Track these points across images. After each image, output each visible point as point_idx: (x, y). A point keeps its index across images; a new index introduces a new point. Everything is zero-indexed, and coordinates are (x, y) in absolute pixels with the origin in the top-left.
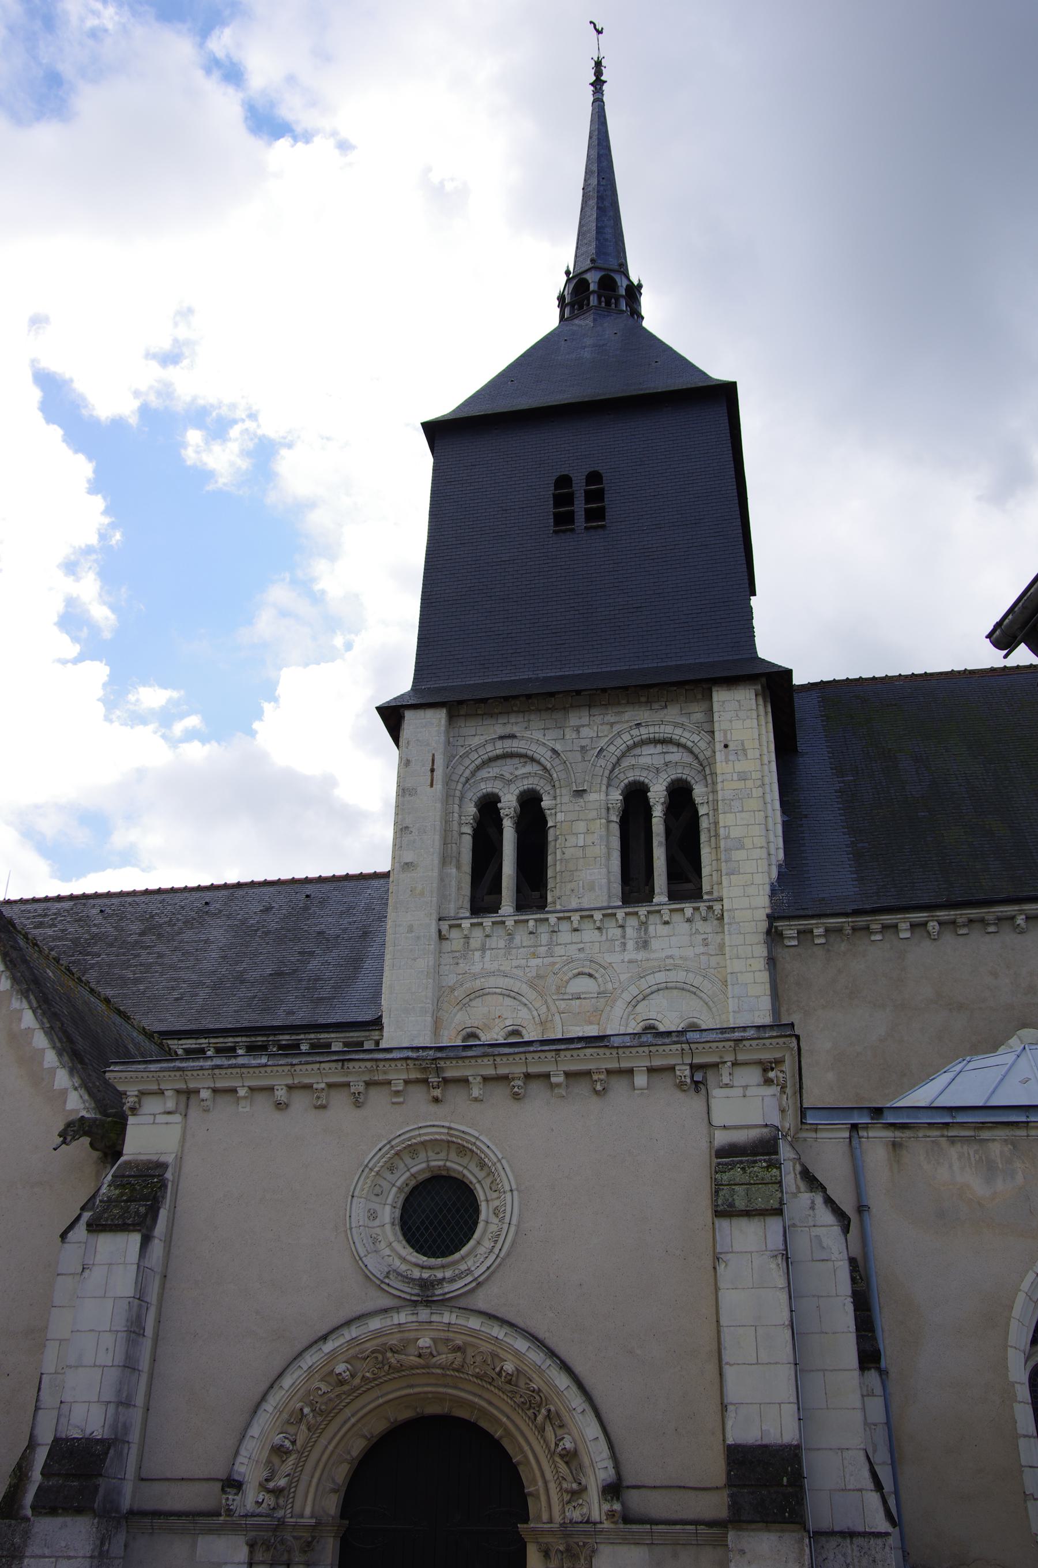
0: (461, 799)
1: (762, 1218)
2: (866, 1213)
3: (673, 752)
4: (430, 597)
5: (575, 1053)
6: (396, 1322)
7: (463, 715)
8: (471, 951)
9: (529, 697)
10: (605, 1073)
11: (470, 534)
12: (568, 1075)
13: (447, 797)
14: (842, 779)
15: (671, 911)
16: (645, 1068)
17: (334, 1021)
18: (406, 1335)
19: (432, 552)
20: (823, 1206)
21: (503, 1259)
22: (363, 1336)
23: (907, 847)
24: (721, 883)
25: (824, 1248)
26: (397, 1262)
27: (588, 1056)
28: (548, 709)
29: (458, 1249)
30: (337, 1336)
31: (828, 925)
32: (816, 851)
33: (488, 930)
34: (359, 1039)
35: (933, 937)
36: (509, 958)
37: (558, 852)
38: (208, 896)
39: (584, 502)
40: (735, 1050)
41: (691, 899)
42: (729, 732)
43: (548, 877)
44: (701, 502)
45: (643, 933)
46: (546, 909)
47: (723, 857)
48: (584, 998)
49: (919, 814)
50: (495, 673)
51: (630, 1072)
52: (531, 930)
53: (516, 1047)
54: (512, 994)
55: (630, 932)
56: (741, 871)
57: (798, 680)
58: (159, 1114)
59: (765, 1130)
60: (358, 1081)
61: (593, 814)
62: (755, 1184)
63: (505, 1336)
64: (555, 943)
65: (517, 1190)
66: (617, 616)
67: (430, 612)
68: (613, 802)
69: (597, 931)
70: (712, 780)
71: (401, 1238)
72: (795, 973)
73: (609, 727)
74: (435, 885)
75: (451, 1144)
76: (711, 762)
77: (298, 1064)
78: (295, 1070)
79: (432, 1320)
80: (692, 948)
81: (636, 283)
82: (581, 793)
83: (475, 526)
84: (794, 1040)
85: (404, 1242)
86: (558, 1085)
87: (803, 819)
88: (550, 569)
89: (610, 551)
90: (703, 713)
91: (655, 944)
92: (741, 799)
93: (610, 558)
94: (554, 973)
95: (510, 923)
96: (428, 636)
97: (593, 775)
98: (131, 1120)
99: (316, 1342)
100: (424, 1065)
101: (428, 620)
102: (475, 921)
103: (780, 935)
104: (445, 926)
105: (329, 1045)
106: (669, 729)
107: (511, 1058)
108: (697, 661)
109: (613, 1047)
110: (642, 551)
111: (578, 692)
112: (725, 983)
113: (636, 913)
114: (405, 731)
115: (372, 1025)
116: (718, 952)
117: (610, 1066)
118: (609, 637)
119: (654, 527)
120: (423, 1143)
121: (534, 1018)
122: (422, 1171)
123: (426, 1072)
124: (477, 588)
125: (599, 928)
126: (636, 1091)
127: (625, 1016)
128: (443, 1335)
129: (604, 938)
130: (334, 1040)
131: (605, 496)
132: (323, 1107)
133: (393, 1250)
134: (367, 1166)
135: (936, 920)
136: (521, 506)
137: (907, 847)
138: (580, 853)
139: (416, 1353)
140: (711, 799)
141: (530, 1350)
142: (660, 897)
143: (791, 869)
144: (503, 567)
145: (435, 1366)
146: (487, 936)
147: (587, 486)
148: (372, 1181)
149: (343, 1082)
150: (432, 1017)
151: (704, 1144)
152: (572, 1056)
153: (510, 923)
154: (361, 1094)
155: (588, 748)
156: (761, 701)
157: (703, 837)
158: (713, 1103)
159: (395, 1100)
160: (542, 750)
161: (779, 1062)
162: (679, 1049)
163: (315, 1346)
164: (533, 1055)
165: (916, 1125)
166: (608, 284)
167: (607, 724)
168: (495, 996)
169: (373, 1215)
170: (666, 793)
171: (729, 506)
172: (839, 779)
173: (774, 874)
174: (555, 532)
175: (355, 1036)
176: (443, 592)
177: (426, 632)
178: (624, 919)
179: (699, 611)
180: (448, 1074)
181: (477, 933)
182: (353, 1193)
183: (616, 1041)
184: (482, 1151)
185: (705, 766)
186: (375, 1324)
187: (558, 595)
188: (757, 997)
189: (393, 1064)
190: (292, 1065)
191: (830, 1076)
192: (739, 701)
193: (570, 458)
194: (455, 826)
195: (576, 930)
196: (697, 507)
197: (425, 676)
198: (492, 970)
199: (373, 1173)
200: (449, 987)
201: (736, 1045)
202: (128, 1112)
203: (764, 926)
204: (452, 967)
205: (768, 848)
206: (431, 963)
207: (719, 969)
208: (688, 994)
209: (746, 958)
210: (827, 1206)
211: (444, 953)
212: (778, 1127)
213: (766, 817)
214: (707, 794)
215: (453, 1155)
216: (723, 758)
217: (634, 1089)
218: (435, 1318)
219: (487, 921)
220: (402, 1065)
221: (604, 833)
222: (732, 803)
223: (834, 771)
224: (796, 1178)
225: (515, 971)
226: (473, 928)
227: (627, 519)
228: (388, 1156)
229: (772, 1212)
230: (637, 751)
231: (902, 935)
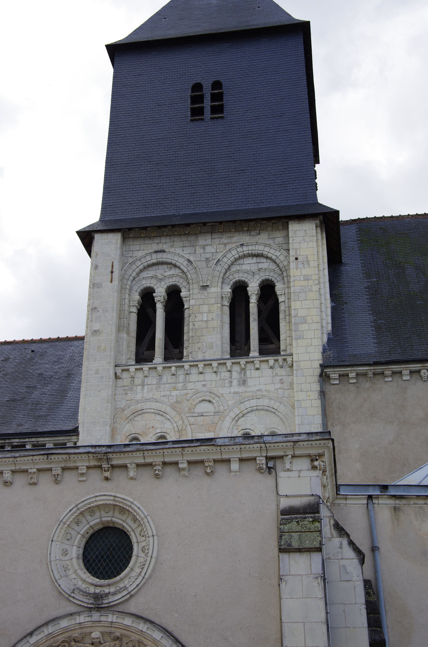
0: (130, 290)
1: (308, 553)
2: (377, 552)
4: (111, 161)
5: (194, 449)
6: (78, 621)
7: (132, 237)
9: (173, 226)
10: (213, 462)
11: (137, 120)
12: (190, 463)
13: (121, 290)
14: (369, 280)
15: (261, 361)
16: (238, 459)
17: (48, 430)
18: (84, 630)
19: (112, 132)
20: (348, 546)
21: (147, 580)
23: (409, 323)
24: (292, 345)
25: (348, 573)
26: (80, 583)
27: (202, 451)
28: (185, 234)
29: (119, 574)
30: (39, 632)
31: (358, 371)
32: (352, 325)
33: (146, 373)
34: (64, 441)
35: (424, 380)
37: (191, 324)
39: (210, 101)
40: (293, 448)
41: (273, 354)
42: (298, 250)
43: (184, 340)
44: (285, 102)
45: (243, 375)
46: (183, 360)
47: (293, 328)
48: (206, 416)
49: (417, 302)
50: (152, 211)
51: (228, 461)
52: (173, 373)
53: (157, 445)
54: (161, 413)
55: (235, 375)
56: (305, 337)
57: (343, 217)
59: (312, 498)
60: (57, 467)
62: (304, 532)
63: (147, 629)
65: (157, 535)
66: (230, 176)
67: (111, 171)
68: (226, 293)
69: (214, 374)
71: (83, 567)
72: (337, 401)
73: (223, 246)
74: (113, 344)
75: (116, 507)
76: (287, 268)
77: (18, 457)
78: (17, 461)
79: (101, 620)
80: (273, 385)
82: (205, 287)
83: (140, 115)
84: (330, 441)
85: (85, 570)
86: (183, 469)
87: (344, 305)
88: (188, 144)
89: (226, 133)
90: (283, 238)
91: (250, 382)
92: (305, 292)
93: (226, 138)
94: (187, 400)
95: (160, 368)
96: (110, 186)
97: (213, 276)
99: (25, 637)
100: (99, 456)
101: (110, 176)
102: (138, 367)
103: (328, 377)
104: (119, 370)
105: (45, 445)
106: (261, 248)
107: (154, 452)
108: (280, 205)
109: (218, 446)
110: (246, 134)
111: (205, 224)
112: (293, 407)
113: (239, 363)
114: (95, 247)
115: (72, 433)
116: (289, 388)
118: (224, 189)
119: (254, 118)
120: (98, 506)
121: (174, 428)
122: (97, 524)
123: (101, 461)
124: (141, 156)
126: (232, 473)
128: (107, 630)
129: (218, 378)
131: (224, 97)
132: (35, 484)
133: (77, 575)
134: (62, 521)
135: (426, 369)
136: (170, 103)
137: (409, 323)
138: (204, 325)
139: (90, 642)
140: (286, 292)
141: (163, 638)
142: (254, 352)
143: (335, 336)
144: (158, 142)
146: (146, 376)
147: (212, 90)
148: (65, 531)
150: (110, 427)
152: (192, 451)
153: (160, 368)
154: (59, 476)
155: (210, 259)
156: (319, 230)
157: (281, 316)
158: (280, 480)
160: (181, 260)
161: (321, 455)
162: (259, 447)
163: (25, 639)
164: (168, 450)
165: (409, 496)
167: (223, 244)
168: (150, 414)
169: (65, 553)
170: (258, 288)
171: (302, 105)
172: (367, 280)
173: (325, 339)
174: (192, 120)
175: (61, 439)
176: (119, 158)
177: (109, 184)
178: (231, 366)
179: (282, 173)
180: (114, 462)
181: (140, 375)
182: (53, 539)
183: (220, 442)
184: (135, 511)
186: (64, 623)
187: (193, 161)
188: (313, 416)
189: (80, 456)
190: (15, 457)
191: (358, 466)
192: (305, 231)
193: (202, 72)
194: (126, 308)
195: (201, 373)
196: (282, 105)
197: (108, 212)
198: (149, 398)
199: (66, 526)
200: (121, 408)
201: (294, 444)
203: (318, 371)
204: (123, 396)
205: (322, 323)
206: (110, 393)
207: (290, 398)
208: (270, 413)
209: (307, 391)
210: (350, 546)
211: (118, 387)
212: (320, 496)
213: (321, 303)
214: (284, 289)
215: (117, 514)
216: (295, 266)
217: (231, 472)
218: (103, 619)
219: (146, 367)
220: (85, 457)
222: (300, 295)
223: (365, 275)
224: (330, 528)
225: (162, 398)
226: (137, 372)
227: (237, 113)
228: (76, 514)
229: (315, 550)
230: (241, 261)
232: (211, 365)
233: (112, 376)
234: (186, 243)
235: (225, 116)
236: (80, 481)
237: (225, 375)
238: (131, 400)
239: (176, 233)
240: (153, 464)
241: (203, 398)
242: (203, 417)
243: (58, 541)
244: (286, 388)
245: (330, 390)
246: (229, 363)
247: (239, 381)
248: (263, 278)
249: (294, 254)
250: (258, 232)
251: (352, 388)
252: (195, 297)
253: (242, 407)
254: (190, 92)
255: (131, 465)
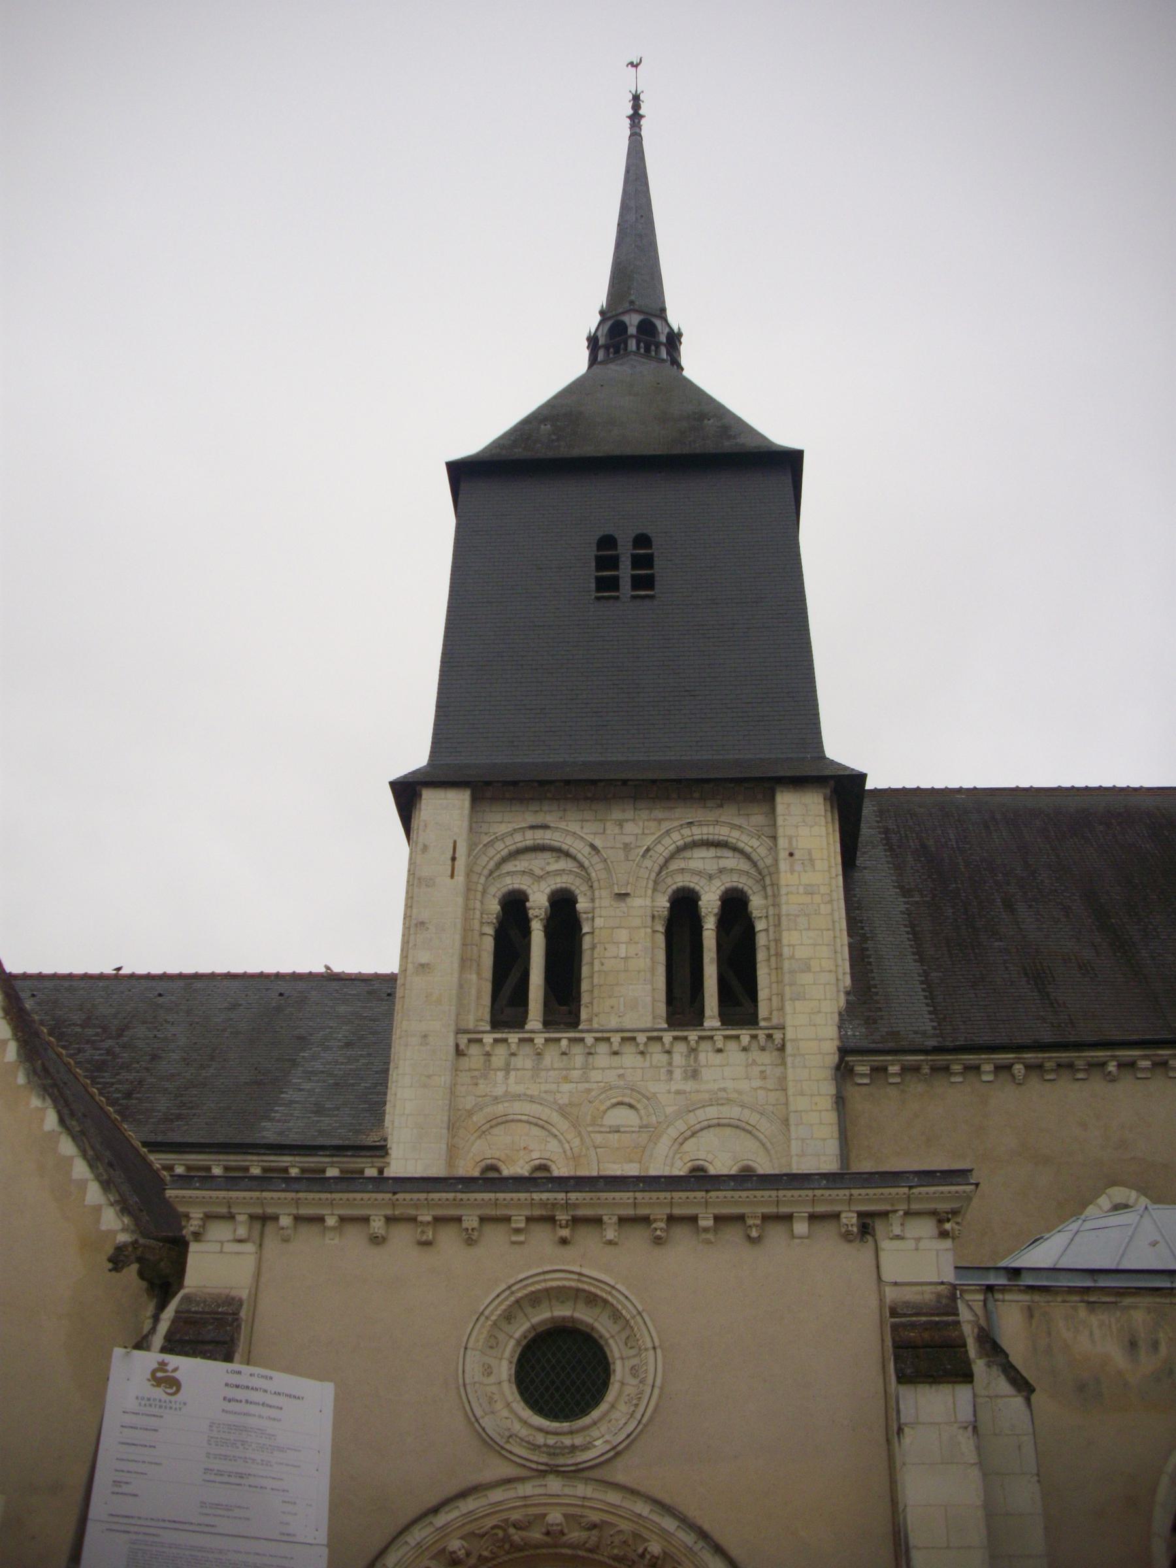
0: (484, 892)
3: (728, 858)
8: (492, 1070)
12: (718, 1219)
15: (726, 1037)
21: (646, 1426)
22: (482, 1509)
26: (517, 1427)
28: (586, 799)
33: (514, 1047)
35: (1017, 1081)
36: (537, 1080)
37: (596, 962)
38: (161, 986)
42: (794, 840)
43: (582, 990)
51: (788, 1218)
52: (564, 1050)
54: (541, 1122)
55: (678, 1059)
56: (807, 997)
57: (869, 785)
58: (228, 1241)
61: (637, 922)
64: (591, 1066)
68: (659, 909)
69: (639, 1055)
70: (773, 892)
74: (454, 992)
81: (676, 330)
86: (706, 1230)
91: (706, 1074)
94: (590, 1102)
95: (539, 1040)
98: (193, 1247)
104: (463, 1040)
111: (625, 782)
112: (786, 1122)
117: (766, 1210)
121: (565, 1152)
125: (642, 1053)
127: (671, 1154)
130: (177, 1162)
131: (655, 563)
132: (427, 1244)
133: (512, 1411)
134: (482, 1313)
145: (565, 1546)
149: (867, 1211)
151: (874, 1303)
153: (539, 1040)
155: (632, 846)
157: (761, 956)
158: (884, 1257)
159: (514, 1238)
166: (647, 329)
169: (488, 1371)
178: (672, 1044)
181: (501, 1051)
185: (766, 877)
186: (497, 1495)
188: (824, 1140)
192: (806, 805)
194: (476, 924)
195: (616, 1053)
199: (490, 1323)
202: (189, 1237)
203: (835, 1059)
208: (743, 1134)
209: (812, 1095)
211: (461, 1071)
214: (767, 908)
221: (649, 945)
230: (687, 854)
231: (985, 1078)
232: (634, 1039)
233: (452, 1050)
234: (588, 815)
235: (657, 596)
236: (514, 1243)
237: (659, 1058)
238: (484, 1096)
239: (570, 796)
240: (652, 1217)
241: (620, 1099)
242: (619, 1134)
243: (476, 1350)
244: (771, 1088)
245: (857, 1097)
246: (668, 1038)
247: (685, 1072)
248: (728, 885)
249: (786, 846)
250: (719, 802)
251: (893, 1092)
252: (604, 913)
253: (692, 1119)
254: (595, 549)
255: (610, 1219)
